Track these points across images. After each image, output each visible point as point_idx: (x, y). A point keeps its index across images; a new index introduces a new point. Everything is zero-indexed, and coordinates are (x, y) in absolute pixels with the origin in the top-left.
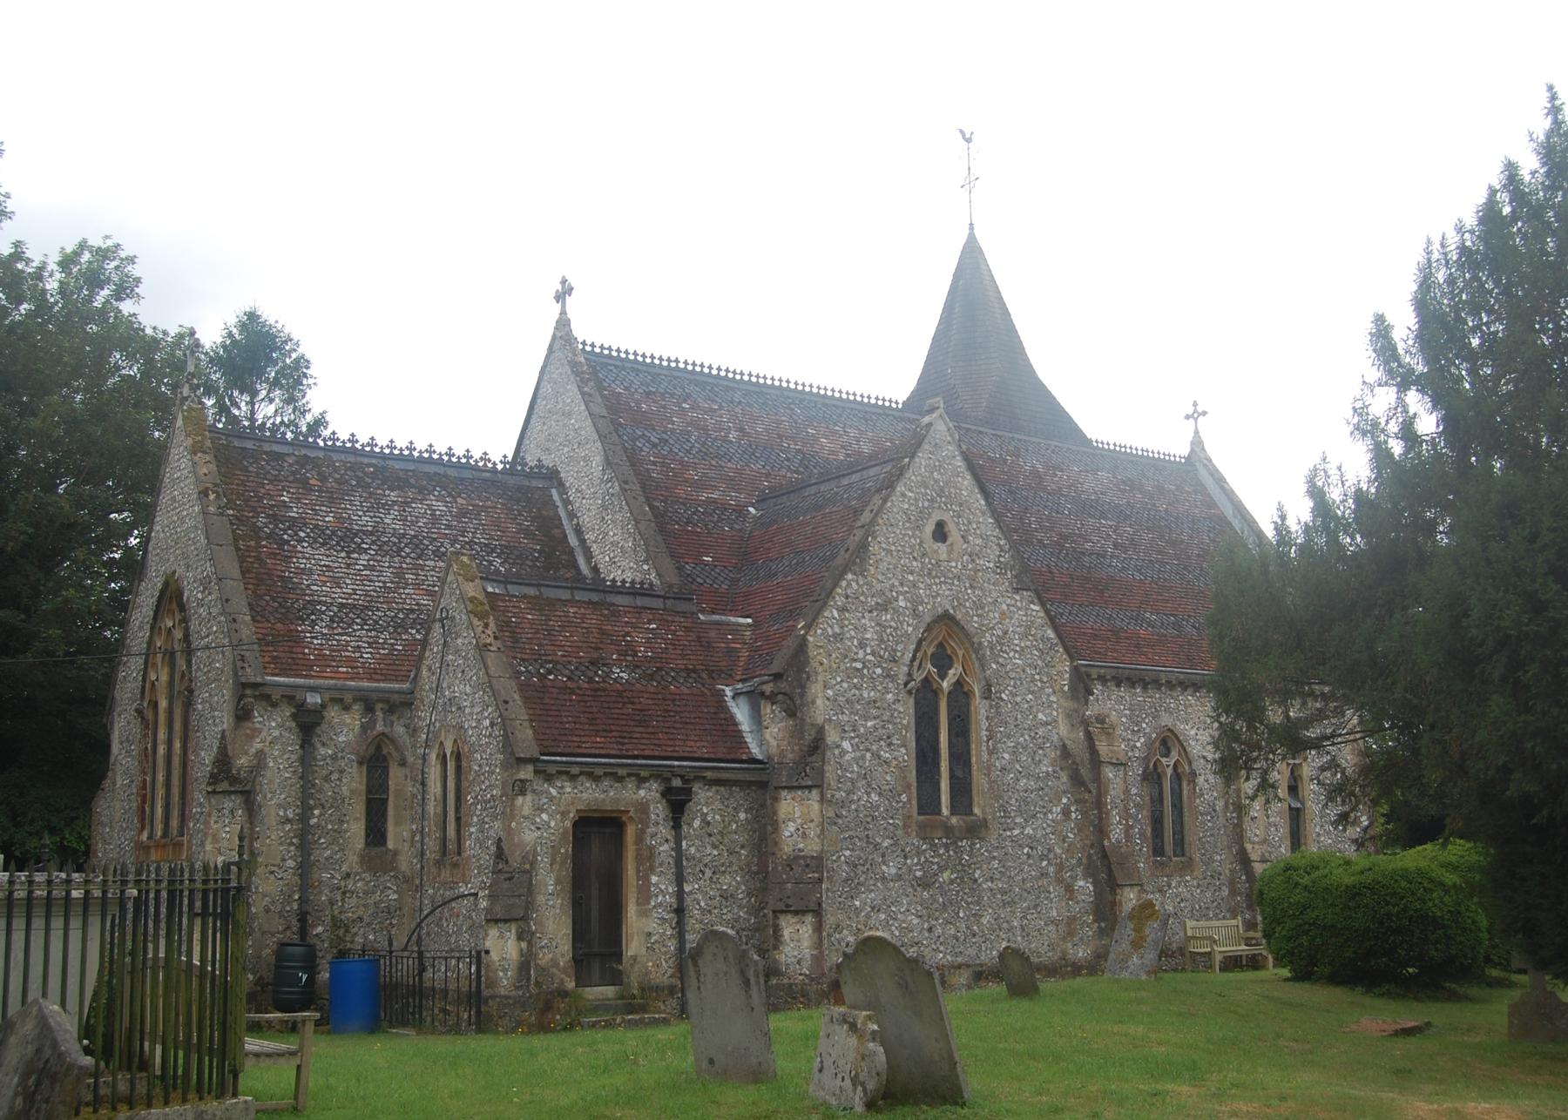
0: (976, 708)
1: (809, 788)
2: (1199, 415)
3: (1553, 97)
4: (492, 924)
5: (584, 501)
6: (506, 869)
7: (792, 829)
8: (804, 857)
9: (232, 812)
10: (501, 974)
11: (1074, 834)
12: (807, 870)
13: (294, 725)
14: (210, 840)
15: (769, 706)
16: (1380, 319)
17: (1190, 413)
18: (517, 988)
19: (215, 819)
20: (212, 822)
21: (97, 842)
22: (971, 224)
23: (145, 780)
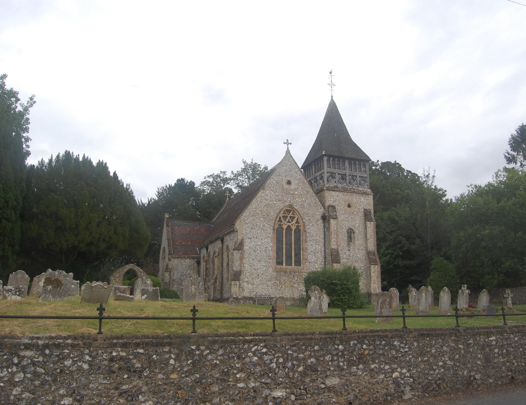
2: (288, 142)
3: (52, 156)
16: (99, 160)
17: (289, 141)
22: (332, 96)
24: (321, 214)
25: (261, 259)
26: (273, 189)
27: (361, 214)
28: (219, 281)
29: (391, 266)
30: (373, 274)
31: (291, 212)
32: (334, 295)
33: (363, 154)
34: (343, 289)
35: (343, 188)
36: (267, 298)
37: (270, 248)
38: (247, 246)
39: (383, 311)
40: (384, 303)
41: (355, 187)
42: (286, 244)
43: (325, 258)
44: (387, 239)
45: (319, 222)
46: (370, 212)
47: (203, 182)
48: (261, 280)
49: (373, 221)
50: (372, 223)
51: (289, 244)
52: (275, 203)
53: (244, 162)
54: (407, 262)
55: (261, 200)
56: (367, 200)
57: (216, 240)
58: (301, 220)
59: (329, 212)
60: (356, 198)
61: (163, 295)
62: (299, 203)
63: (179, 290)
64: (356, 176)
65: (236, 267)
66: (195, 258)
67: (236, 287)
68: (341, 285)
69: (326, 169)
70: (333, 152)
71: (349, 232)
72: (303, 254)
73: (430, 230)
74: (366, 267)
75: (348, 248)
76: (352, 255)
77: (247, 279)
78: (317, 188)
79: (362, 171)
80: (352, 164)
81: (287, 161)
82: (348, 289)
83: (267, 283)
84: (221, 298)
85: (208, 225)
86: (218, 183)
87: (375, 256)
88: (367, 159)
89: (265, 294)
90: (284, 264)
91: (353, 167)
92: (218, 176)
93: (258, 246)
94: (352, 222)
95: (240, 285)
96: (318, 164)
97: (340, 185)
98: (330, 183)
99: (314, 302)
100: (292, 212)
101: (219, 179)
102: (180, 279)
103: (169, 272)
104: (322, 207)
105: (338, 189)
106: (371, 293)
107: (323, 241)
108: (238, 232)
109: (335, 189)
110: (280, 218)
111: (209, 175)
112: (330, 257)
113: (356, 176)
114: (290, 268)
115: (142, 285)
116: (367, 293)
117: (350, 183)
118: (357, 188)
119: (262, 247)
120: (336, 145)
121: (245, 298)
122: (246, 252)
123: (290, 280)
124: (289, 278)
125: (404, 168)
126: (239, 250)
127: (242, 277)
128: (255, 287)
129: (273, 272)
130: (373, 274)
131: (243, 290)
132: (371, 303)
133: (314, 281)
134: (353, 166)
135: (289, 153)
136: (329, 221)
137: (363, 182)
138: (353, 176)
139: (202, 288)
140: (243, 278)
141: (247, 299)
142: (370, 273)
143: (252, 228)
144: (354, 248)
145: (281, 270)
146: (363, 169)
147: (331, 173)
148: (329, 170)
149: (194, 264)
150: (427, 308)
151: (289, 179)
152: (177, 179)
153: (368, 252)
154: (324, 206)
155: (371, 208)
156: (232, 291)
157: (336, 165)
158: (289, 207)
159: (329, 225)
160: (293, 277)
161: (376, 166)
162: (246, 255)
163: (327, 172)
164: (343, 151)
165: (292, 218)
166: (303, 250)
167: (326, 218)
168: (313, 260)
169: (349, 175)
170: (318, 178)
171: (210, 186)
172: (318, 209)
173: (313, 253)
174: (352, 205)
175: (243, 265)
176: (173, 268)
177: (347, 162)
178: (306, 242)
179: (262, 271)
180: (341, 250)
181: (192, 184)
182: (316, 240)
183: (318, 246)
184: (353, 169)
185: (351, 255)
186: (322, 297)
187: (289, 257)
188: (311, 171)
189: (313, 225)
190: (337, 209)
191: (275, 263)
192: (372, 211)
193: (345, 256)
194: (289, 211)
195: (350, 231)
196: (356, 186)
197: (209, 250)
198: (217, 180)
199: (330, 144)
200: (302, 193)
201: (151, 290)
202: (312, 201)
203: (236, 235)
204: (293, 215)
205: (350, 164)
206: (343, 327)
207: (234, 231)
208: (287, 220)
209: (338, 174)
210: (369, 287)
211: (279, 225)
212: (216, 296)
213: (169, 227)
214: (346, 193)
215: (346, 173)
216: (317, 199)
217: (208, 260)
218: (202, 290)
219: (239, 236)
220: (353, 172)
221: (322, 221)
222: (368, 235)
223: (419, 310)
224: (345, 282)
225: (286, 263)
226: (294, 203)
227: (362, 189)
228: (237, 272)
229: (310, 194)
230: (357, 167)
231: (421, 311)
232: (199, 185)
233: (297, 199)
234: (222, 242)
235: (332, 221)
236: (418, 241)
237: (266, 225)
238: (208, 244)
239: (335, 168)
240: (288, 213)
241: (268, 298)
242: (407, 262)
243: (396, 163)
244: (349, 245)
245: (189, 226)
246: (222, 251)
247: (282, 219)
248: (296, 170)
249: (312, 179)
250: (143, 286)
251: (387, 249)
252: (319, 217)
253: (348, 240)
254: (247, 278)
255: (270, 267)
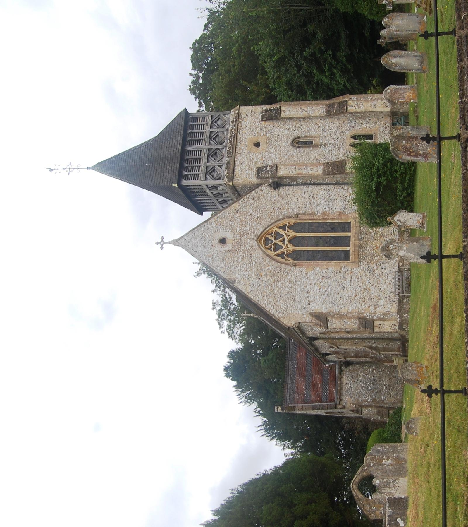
22: (88, 168)
24: (270, 190)
25: (341, 286)
26: (233, 267)
27: (269, 125)
28: (375, 343)
29: (349, 67)
30: (362, 109)
31: (268, 238)
32: (394, 186)
33: (176, 121)
34: (385, 173)
35: (230, 154)
36: (399, 277)
37: (324, 272)
38: (321, 308)
39: (421, 152)
40: (408, 150)
41: (227, 134)
42: (317, 246)
43: (337, 184)
44: (307, 72)
45: (282, 193)
46: (266, 111)
47: (229, 334)
48: (373, 285)
49: (280, 107)
50: (283, 108)
51: (318, 241)
52: (254, 263)
53: (199, 274)
54: (343, 42)
55: (250, 286)
56: (247, 115)
57: (313, 346)
58: (280, 222)
59: (266, 178)
60: (245, 133)
61: (397, 433)
62: (253, 225)
63: (388, 392)
64: (211, 133)
65: (353, 324)
66: (341, 368)
67: (384, 324)
68: (379, 177)
69: (200, 182)
70: (174, 169)
71: (297, 145)
72: (332, 219)
73: (293, 6)
74: (351, 119)
75: (322, 148)
76: (333, 141)
77: (371, 308)
78: (229, 194)
79: (203, 123)
80: (192, 140)
81: (189, 244)
82: (385, 165)
83: (376, 275)
84: (400, 340)
85: (291, 347)
86: (230, 313)
87: (334, 104)
88: (184, 115)
89: (393, 278)
90: (348, 248)
91: (197, 138)
92: (220, 312)
93: (321, 290)
94: (281, 140)
95: (380, 319)
96: (194, 192)
97: (225, 160)
98: (222, 175)
99: (407, 251)
100: (267, 236)
101: (224, 312)
102: (373, 392)
103: (362, 408)
104: (260, 188)
105: (232, 163)
106: (390, 111)
107: (311, 188)
108: (299, 321)
109: (232, 168)
110: (277, 255)
111: (219, 326)
112: (337, 176)
113: (211, 133)
114: (354, 239)
115: (382, 493)
116: (390, 116)
117: (221, 144)
118: (229, 131)
119: (322, 284)
120: (163, 165)
121: (400, 310)
122: (331, 309)
123: (371, 239)
124: (368, 241)
125: (200, 36)
126: (327, 321)
127: (368, 316)
128: (384, 295)
129: (360, 266)
130: (362, 107)
131: (388, 313)
132: (406, 112)
133: (374, 217)
134: (195, 138)
135: (177, 240)
136: (282, 178)
137: (219, 122)
138: (210, 138)
139: (385, 448)
140: (370, 314)
141: (401, 307)
142: (360, 112)
143: (294, 300)
144: (322, 137)
145: (357, 254)
146: (199, 122)
147: (207, 173)
148: (202, 176)
149: (349, 371)
150: (416, 54)
151: (218, 241)
152: (225, 378)
153: (328, 116)
154: (258, 186)
155: (259, 109)
156: (390, 330)
157: (194, 165)
158: (260, 241)
159: (286, 178)
160: (367, 234)
161: (198, 78)
162: (335, 309)
163: (205, 180)
164: (172, 153)
165: (277, 235)
166: (325, 219)
167: (277, 182)
168: (341, 204)
169: (210, 144)
170: (215, 192)
171: (234, 326)
172: (263, 195)
173: (330, 203)
174: (255, 141)
175: (350, 313)
176: (356, 402)
177: (190, 148)
178: (313, 214)
179: (359, 284)
180: (325, 158)
181: (232, 355)
182: (311, 198)
183: (319, 196)
184: (199, 138)
185: (333, 142)
186: (399, 223)
187: (337, 241)
188: (206, 201)
189: (287, 203)
190: (263, 165)
191: (346, 262)
192: (265, 108)
193: (335, 153)
194: (267, 240)
195: (296, 143)
196: (225, 133)
197: (328, 352)
198: (226, 314)
199: (162, 174)
200: (239, 220)
201: (391, 510)
202: (251, 205)
203: (305, 323)
204: (273, 235)
205: (192, 142)
206: (461, 394)
207: (299, 328)
208: (280, 244)
209: (207, 162)
210: (381, 114)
211: (291, 229)
212: (396, 347)
213: (295, 407)
214: (237, 150)
215: (206, 149)
216: (247, 196)
217: (343, 354)
218: (389, 447)
219: (305, 319)
220: (204, 138)
221: (281, 188)
222: (302, 115)
223: (418, 69)
224: (374, 170)
225: (347, 246)
226: (254, 232)
227: (231, 123)
228: (361, 324)
229: (240, 207)
230: (196, 131)
231: (421, 65)
232: (234, 341)
233: (248, 229)
234: (317, 339)
235: (282, 172)
236: (311, 28)
237: (288, 278)
238: (320, 354)
239: (199, 167)
240: (270, 242)
241: (399, 276)
242: (343, 42)
243: (194, 48)
244: (317, 146)
245: (294, 376)
246: (329, 338)
247: (279, 251)
248: (202, 229)
249: (217, 200)
250: (383, 491)
251: (322, 72)
252: (275, 193)
253: (309, 147)
254: (369, 307)
255: (352, 271)
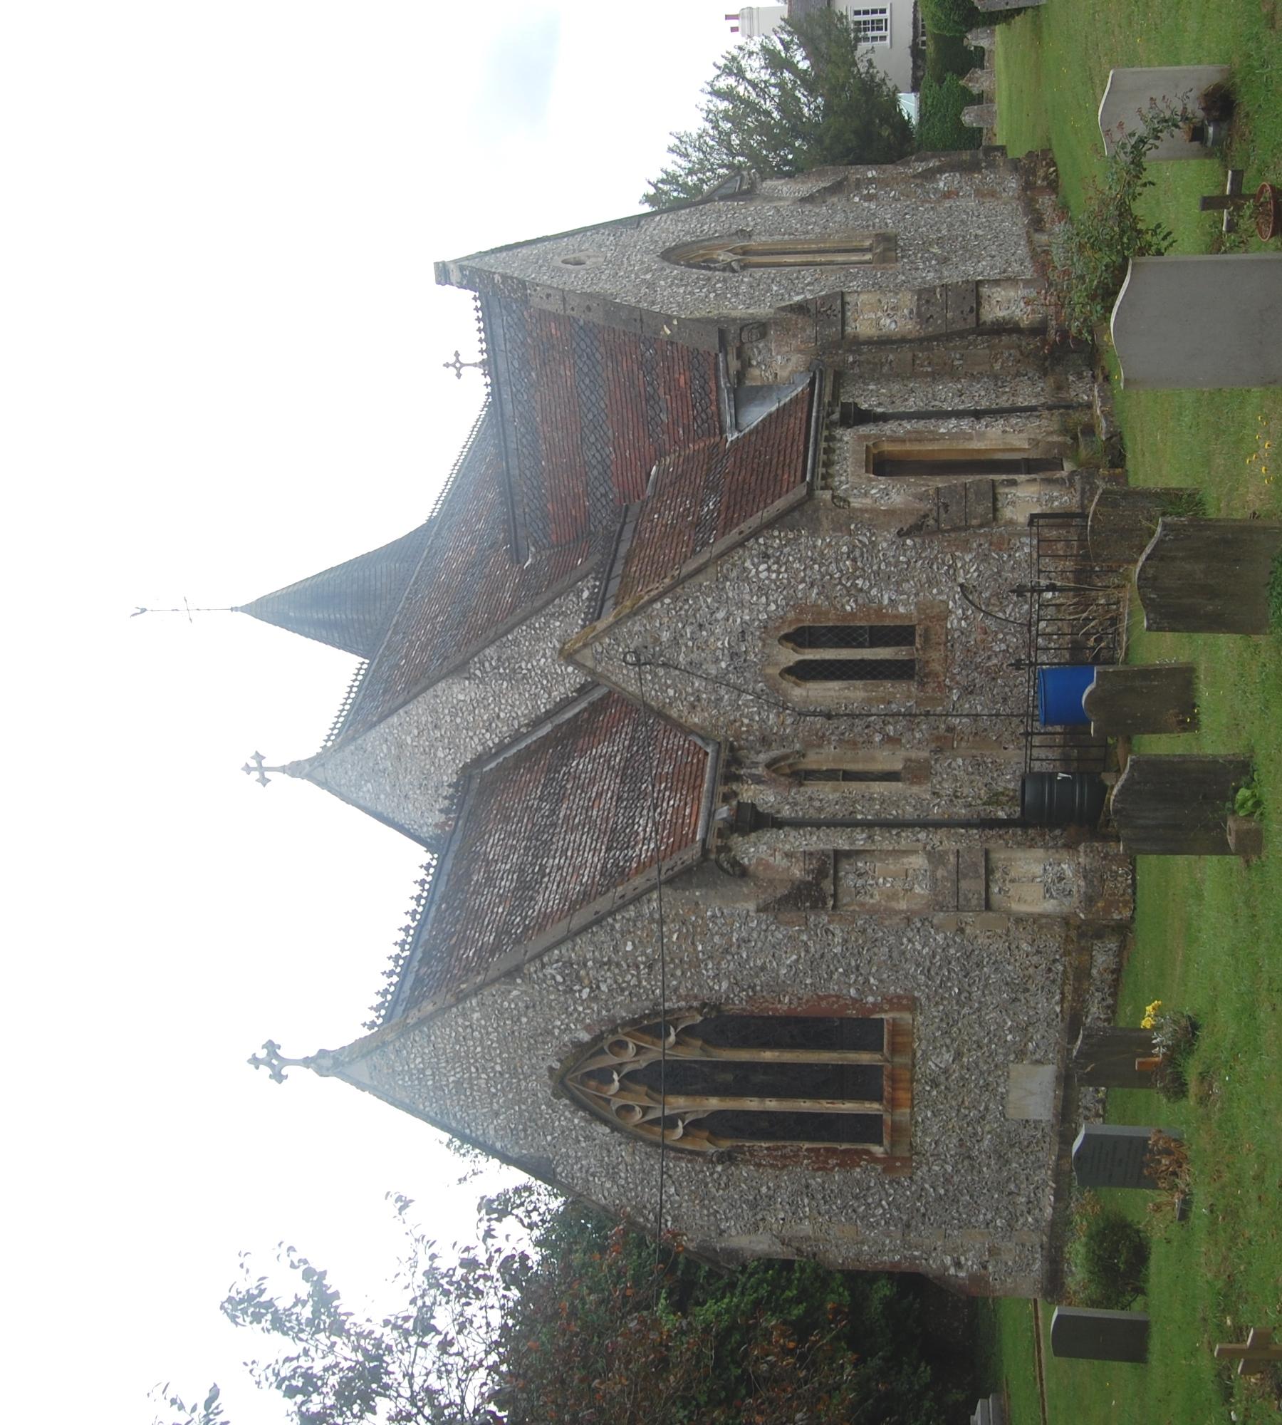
0: (759, 245)
1: (844, 304)
4: (999, 515)
5: (502, 715)
6: (935, 514)
7: (888, 321)
8: (919, 307)
9: (860, 875)
10: (1056, 503)
11: (891, 190)
12: (933, 300)
13: (753, 834)
14: (894, 905)
15: (756, 372)
18: (1072, 485)
19: (867, 898)
20: (871, 901)
21: (882, 1262)
22: (232, 609)
23: (807, 1150)
